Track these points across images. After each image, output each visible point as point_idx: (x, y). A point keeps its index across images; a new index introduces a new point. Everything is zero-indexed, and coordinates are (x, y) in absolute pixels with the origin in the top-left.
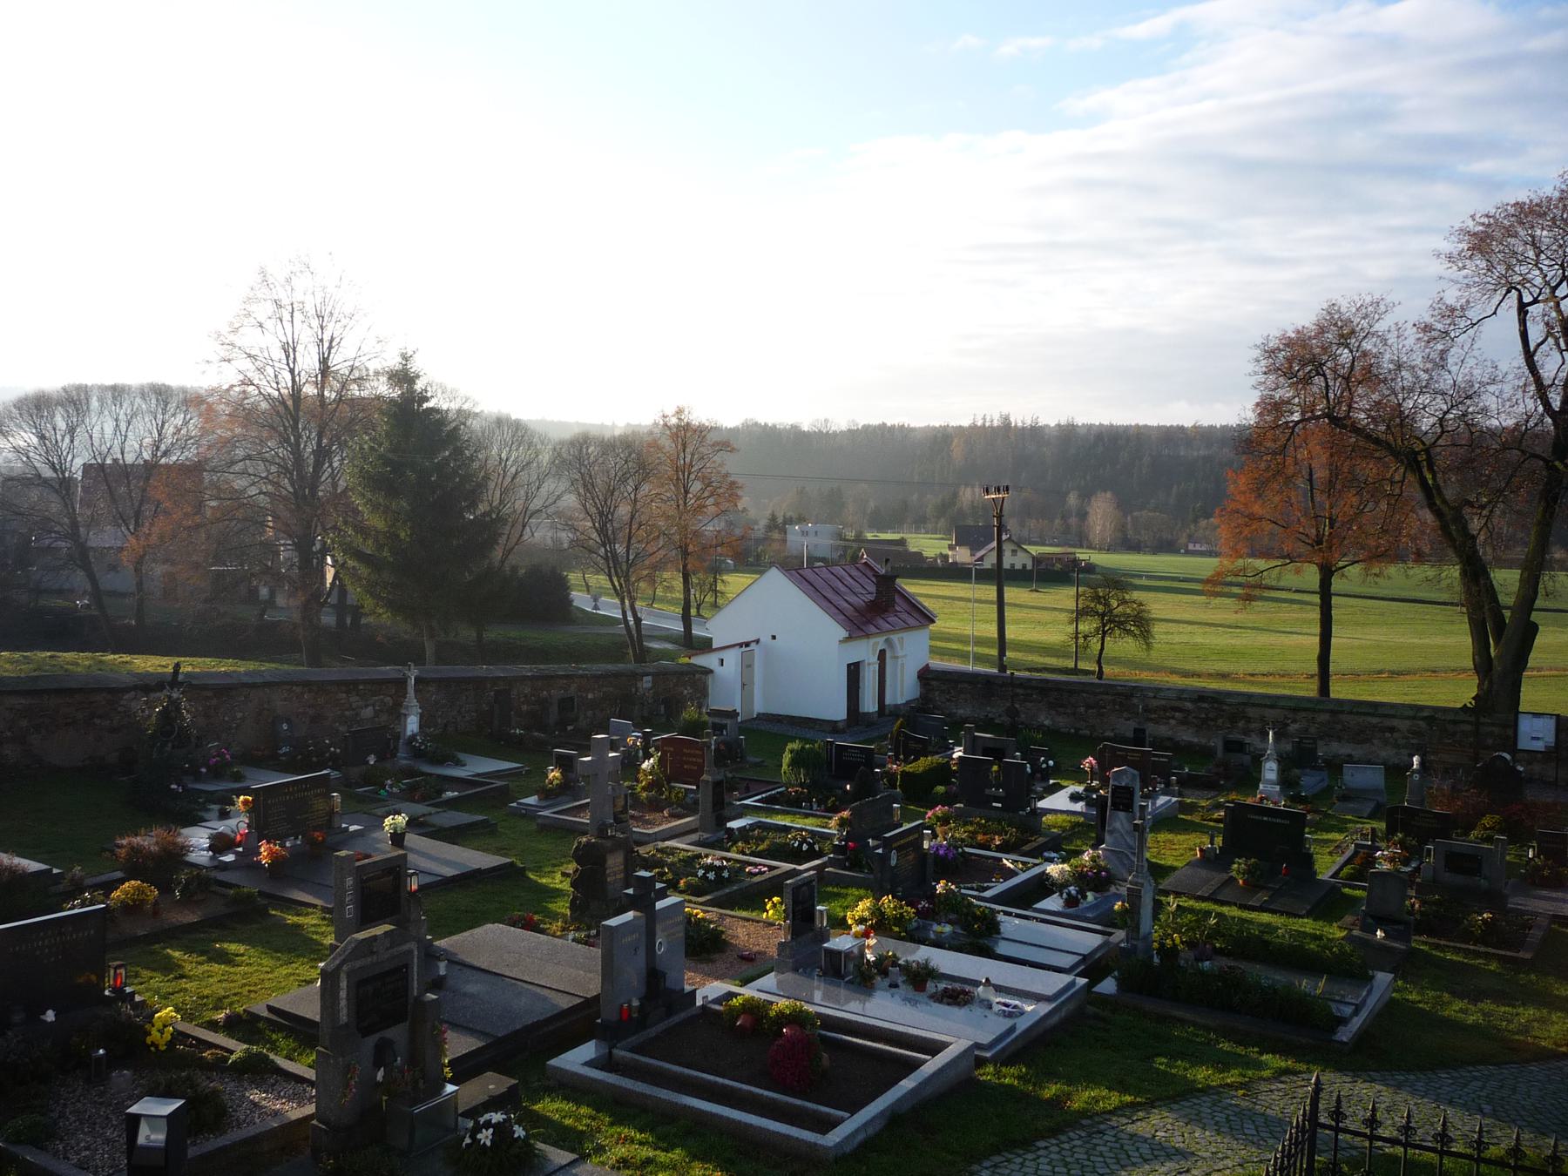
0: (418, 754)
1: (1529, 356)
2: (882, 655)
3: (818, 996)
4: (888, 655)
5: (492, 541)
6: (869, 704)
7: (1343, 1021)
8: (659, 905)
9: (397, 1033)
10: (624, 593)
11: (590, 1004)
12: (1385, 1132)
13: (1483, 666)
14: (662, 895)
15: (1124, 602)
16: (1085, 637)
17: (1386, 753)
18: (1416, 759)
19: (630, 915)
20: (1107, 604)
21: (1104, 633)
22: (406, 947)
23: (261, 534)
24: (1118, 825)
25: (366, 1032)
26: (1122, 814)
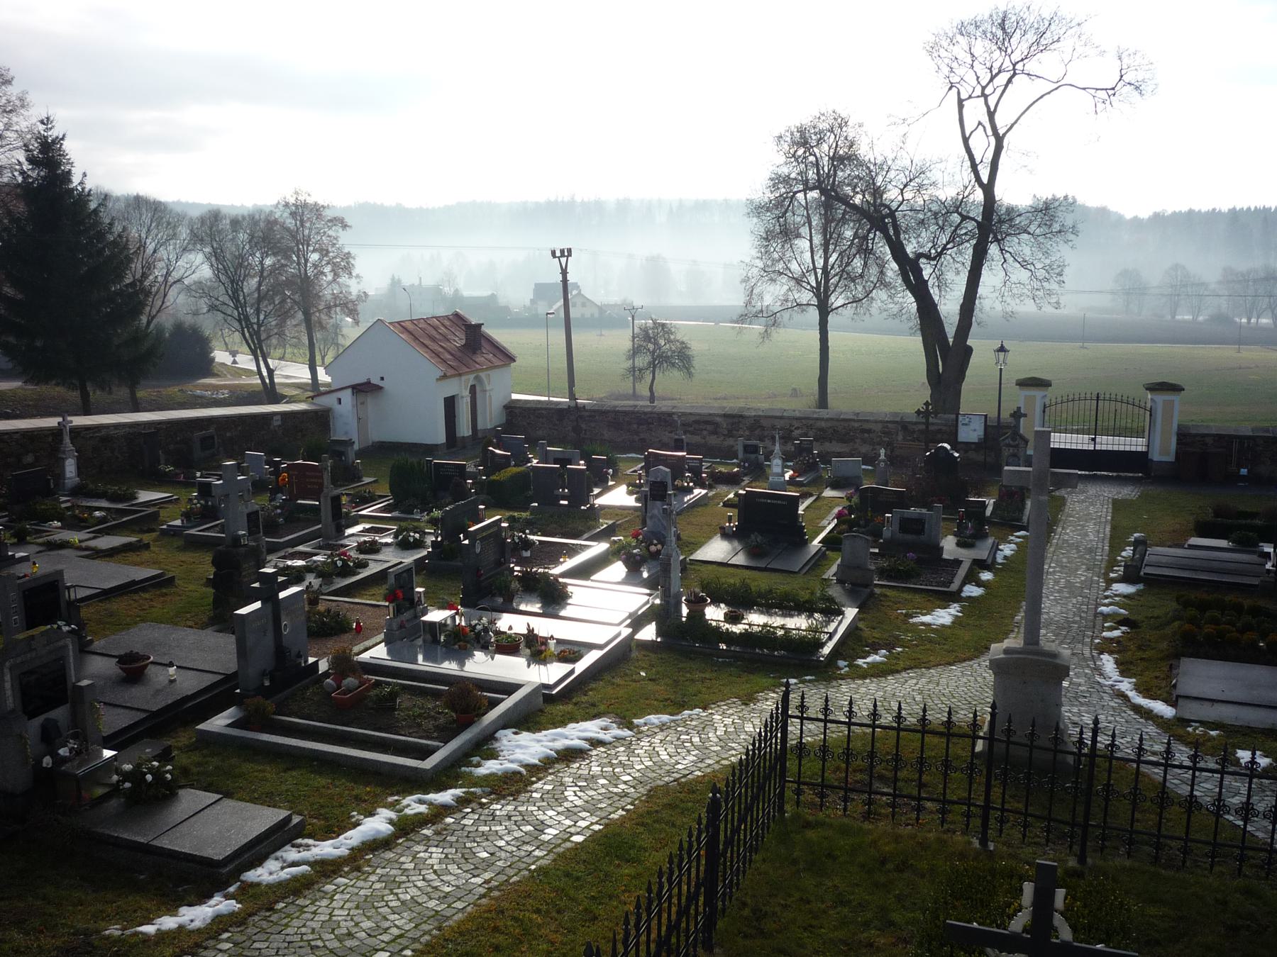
0: (685, 566)
1: (966, 140)
2: (473, 390)
3: (420, 658)
4: (478, 389)
5: (137, 310)
6: (464, 429)
7: (822, 645)
8: (282, 595)
9: (59, 714)
10: (258, 350)
11: (229, 678)
12: (883, 721)
13: (934, 377)
14: (285, 586)
15: (669, 341)
16: (640, 370)
17: (865, 449)
18: (882, 451)
19: (258, 605)
20: (656, 343)
21: (654, 367)
22: (61, 643)
23: (787, 457)
24: (656, 512)
25: (32, 715)
26: (658, 503)
